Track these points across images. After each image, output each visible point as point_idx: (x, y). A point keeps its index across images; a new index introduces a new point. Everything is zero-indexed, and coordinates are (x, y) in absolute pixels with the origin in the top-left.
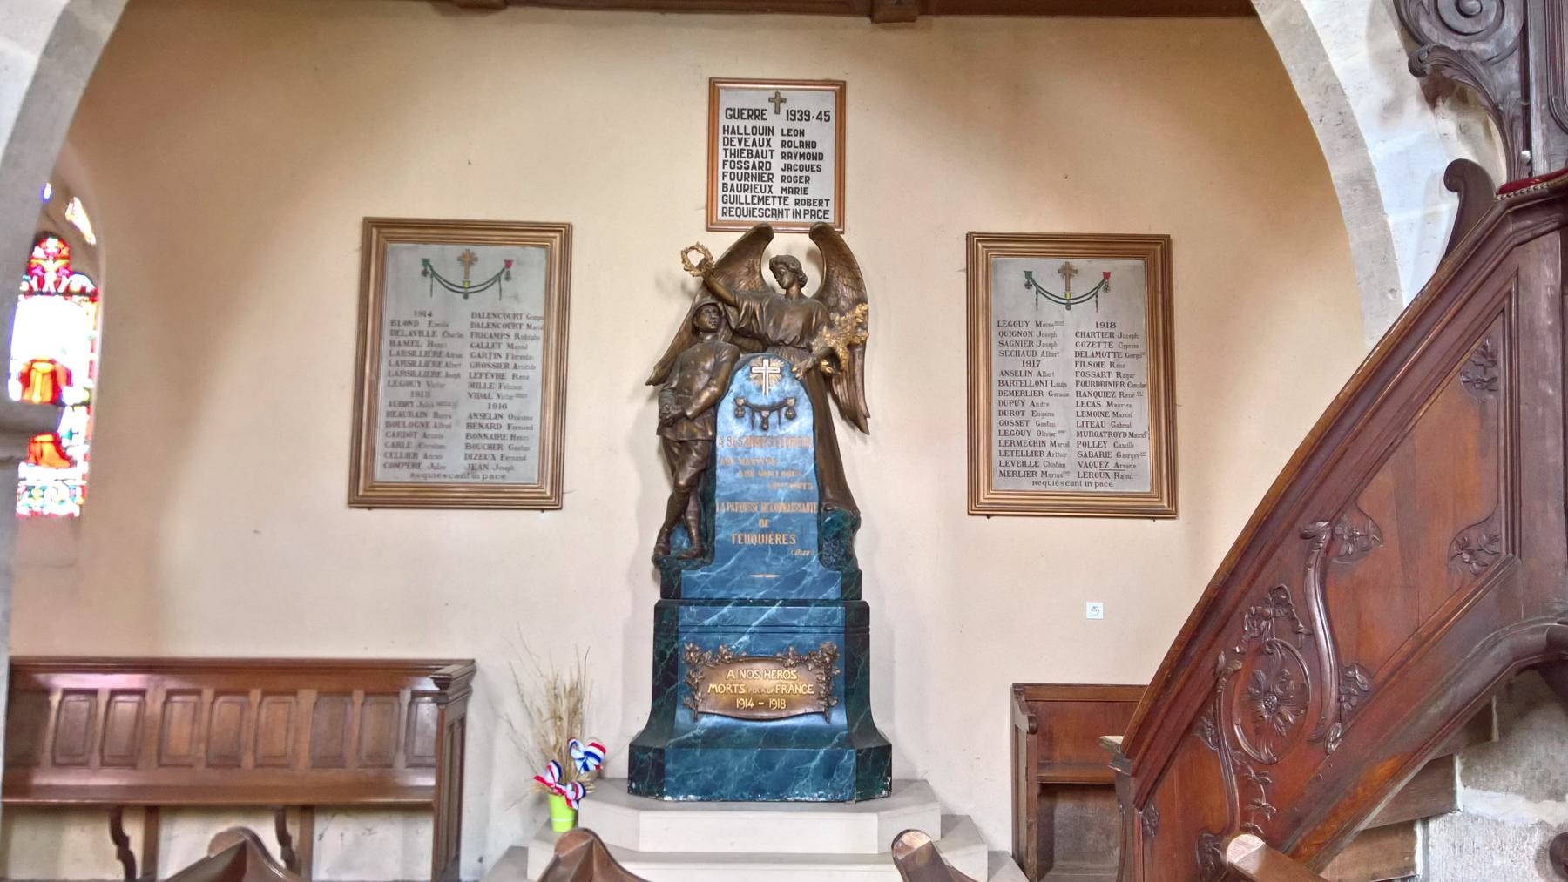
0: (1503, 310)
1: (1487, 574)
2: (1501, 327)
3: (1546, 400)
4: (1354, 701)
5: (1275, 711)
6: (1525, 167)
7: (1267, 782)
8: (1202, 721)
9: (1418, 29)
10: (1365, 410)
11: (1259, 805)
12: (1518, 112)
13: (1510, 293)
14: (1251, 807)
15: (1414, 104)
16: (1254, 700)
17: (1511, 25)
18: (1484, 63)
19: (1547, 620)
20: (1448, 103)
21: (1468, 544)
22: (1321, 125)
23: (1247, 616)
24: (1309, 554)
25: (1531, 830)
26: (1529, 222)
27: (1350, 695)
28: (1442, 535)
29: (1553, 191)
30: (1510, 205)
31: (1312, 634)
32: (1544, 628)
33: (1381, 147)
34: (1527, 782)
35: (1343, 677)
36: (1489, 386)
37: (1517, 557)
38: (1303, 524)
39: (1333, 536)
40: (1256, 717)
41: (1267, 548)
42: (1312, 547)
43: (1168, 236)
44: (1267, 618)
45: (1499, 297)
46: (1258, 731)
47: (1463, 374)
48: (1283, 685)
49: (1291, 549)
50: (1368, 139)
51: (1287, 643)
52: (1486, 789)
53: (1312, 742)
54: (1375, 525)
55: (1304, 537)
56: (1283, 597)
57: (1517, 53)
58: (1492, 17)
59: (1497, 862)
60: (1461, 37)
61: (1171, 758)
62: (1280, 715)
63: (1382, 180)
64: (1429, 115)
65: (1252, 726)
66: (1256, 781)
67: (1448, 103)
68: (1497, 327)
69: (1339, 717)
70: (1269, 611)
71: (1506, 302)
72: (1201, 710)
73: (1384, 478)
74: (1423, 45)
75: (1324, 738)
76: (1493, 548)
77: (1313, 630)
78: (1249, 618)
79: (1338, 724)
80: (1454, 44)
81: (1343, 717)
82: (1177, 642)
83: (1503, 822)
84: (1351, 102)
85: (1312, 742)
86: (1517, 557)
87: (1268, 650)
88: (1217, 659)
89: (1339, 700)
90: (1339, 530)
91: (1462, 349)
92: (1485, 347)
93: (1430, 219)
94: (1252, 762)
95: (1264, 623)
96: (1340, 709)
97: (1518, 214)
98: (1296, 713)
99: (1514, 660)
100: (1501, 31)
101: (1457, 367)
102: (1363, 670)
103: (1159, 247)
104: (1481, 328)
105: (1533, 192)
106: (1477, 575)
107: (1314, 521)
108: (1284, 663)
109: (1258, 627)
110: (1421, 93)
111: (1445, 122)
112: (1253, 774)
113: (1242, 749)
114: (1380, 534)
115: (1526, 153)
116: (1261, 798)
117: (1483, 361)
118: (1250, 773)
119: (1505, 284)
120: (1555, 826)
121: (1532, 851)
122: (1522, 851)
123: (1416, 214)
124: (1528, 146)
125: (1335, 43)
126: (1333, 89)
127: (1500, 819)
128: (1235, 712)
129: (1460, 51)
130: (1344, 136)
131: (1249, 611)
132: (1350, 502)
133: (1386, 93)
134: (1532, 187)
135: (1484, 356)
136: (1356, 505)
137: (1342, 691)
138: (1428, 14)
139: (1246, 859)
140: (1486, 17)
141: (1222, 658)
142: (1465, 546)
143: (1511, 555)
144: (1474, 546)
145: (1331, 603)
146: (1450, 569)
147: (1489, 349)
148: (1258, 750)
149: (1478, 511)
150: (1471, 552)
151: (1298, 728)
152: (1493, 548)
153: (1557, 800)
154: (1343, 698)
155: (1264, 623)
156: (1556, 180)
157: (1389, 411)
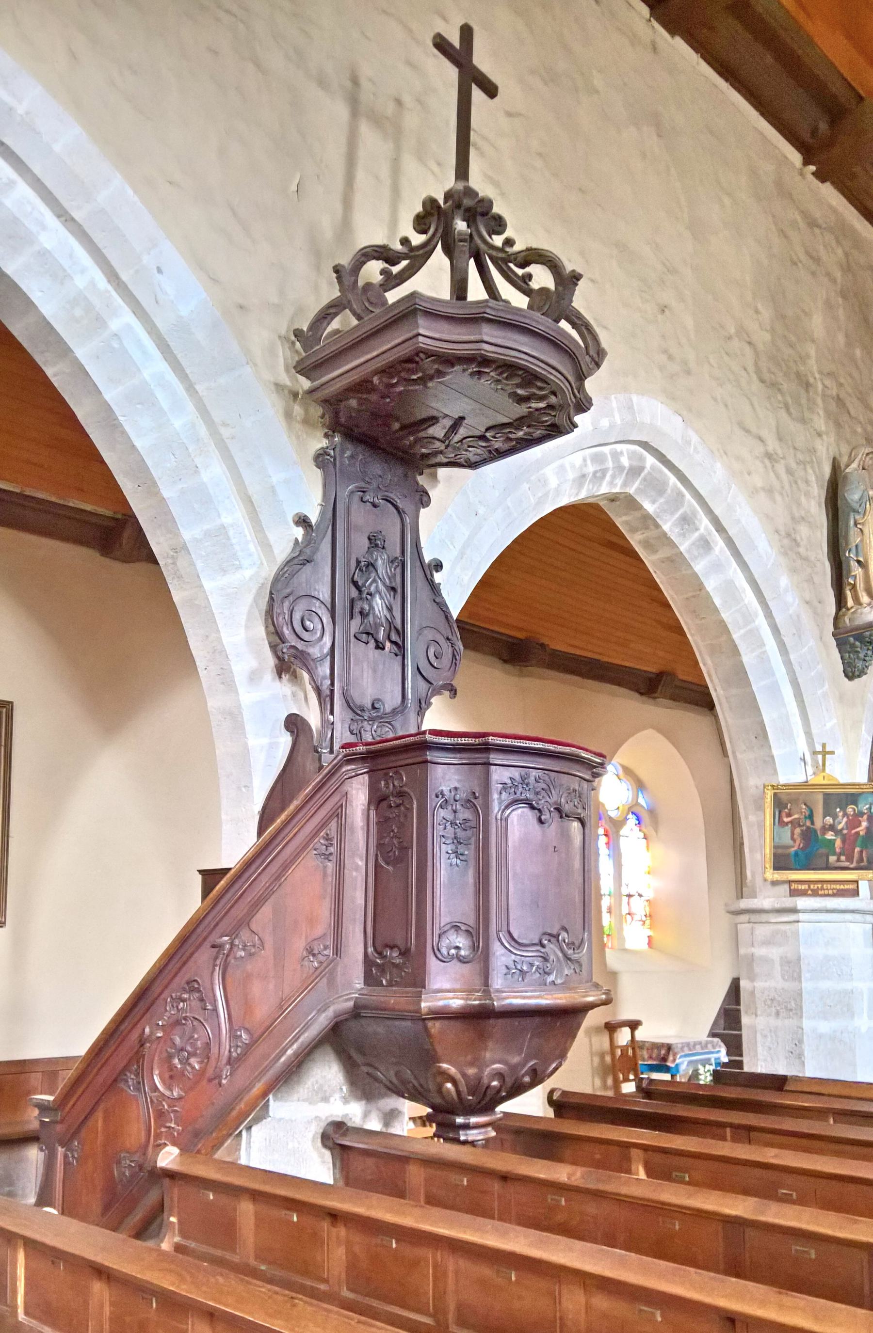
0: (337, 815)
1: (322, 968)
2: (336, 824)
3: (357, 869)
4: (239, 1050)
5: (185, 1062)
6: (330, 726)
7: (176, 1111)
8: (125, 1075)
9: (283, 633)
10: (258, 868)
11: (169, 1127)
12: (328, 692)
13: (342, 804)
14: (163, 1130)
15: (269, 675)
16: (170, 1057)
17: (327, 640)
18: (313, 660)
19: (353, 993)
20: (287, 676)
21: (312, 950)
22: (205, 672)
23: (169, 1000)
24: (216, 958)
25: (309, 1122)
26: (353, 767)
27: (237, 1046)
28: (299, 945)
29: (369, 752)
30: (345, 756)
31: (215, 1009)
32: (352, 998)
33: (248, 696)
34: (310, 1094)
35: (233, 1036)
36: (327, 857)
37: (338, 958)
38: (214, 938)
39: (232, 944)
40: (171, 1068)
41: (187, 954)
42: (218, 953)
43: (12, 703)
44: (184, 1001)
45: (336, 807)
46: (172, 1077)
47: (315, 850)
48: (193, 1045)
49: (204, 956)
50: (241, 690)
51: (197, 1017)
52: (286, 1101)
53: (210, 1080)
54: (260, 939)
55: (213, 946)
56: (196, 986)
57: (329, 657)
58: (318, 634)
59: (290, 1146)
60: (302, 642)
61: (97, 1103)
62: (190, 1064)
63: (246, 715)
64: (277, 683)
65: (167, 1076)
66: (168, 1111)
67: (287, 676)
68: (333, 824)
69: (229, 1062)
70: (186, 996)
71: (340, 810)
72: (126, 1068)
73: (266, 910)
74: (284, 643)
75: (219, 1077)
76: (325, 953)
77: (216, 1006)
78: (170, 1001)
79: (228, 1067)
80: (300, 645)
81: (232, 1062)
82: (113, 1021)
83: (295, 1120)
84: (232, 663)
85: (210, 1080)
86: (338, 958)
87: (183, 1022)
88: (144, 1030)
89: (230, 1051)
90: (237, 942)
91: (315, 834)
92: (327, 835)
93: (272, 746)
94: (166, 1099)
95: (181, 1004)
96: (230, 1058)
97: (349, 762)
98: (200, 1063)
99: (336, 1017)
100: (322, 643)
101: (311, 846)
102: (247, 1031)
103: (4, 710)
104: (324, 824)
105: (359, 751)
106: (316, 968)
107: (222, 936)
108: (194, 1029)
109: (177, 1007)
110: (275, 669)
111: (284, 688)
112: (166, 1107)
113: (160, 1091)
114: (262, 944)
115: (331, 717)
116: (171, 1122)
117: (326, 843)
118: (164, 1106)
119: (339, 800)
120: (324, 1118)
121: (310, 1135)
122: (305, 1137)
123: (265, 741)
124: (332, 713)
125: (225, 624)
126: (219, 652)
127: (293, 1119)
128: (155, 1066)
129: (302, 651)
130: (223, 683)
131: (171, 996)
132: (245, 922)
133: (254, 664)
134: (358, 748)
135: (327, 840)
136: (249, 928)
137: (232, 1045)
138: (287, 624)
139: (172, 1162)
140: (316, 633)
141: (147, 1030)
142: (311, 952)
143: (335, 956)
144: (316, 952)
145: (228, 989)
146: (302, 965)
147: (330, 837)
148: (171, 1091)
149: (319, 931)
150: (314, 955)
151: (203, 1071)
152: (325, 953)
153: (325, 1102)
154: (232, 1050)
155: (181, 1004)
156: (371, 747)
157: (274, 868)
